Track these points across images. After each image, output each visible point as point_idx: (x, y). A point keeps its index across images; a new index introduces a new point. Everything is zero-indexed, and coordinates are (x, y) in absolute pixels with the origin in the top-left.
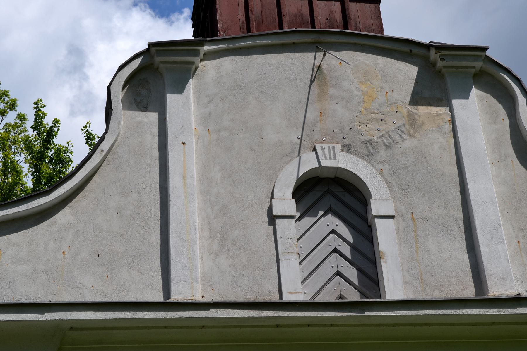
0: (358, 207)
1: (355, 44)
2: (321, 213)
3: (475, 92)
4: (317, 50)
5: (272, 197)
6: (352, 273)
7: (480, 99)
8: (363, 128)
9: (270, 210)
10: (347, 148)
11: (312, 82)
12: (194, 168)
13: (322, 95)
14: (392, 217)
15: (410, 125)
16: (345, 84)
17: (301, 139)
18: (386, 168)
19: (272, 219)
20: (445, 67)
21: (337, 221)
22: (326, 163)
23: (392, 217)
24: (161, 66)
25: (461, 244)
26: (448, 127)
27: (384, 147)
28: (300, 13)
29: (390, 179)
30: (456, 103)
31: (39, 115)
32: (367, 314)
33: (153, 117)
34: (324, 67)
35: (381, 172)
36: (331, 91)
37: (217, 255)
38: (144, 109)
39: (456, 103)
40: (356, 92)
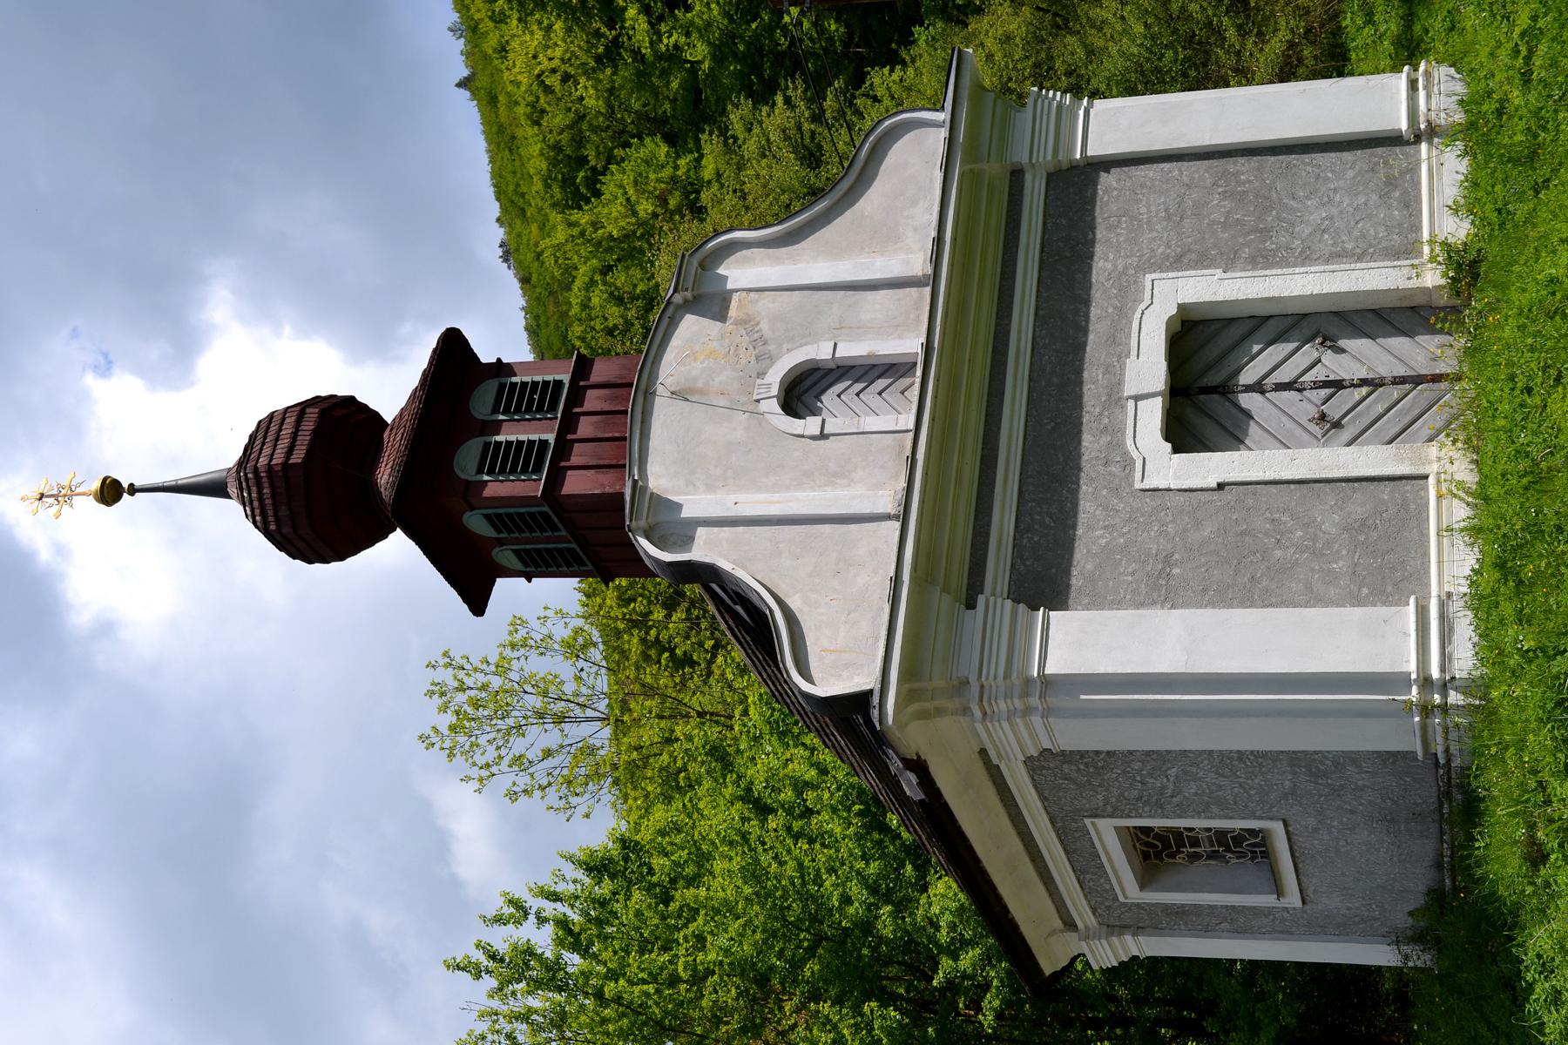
0: (817, 375)
1: (653, 362)
2: (819, 404)
3: (721, 271)
4: (654, 393)
5: (803, 436)
6: (881, 383)
7: (728, 268)
8: (743, 362)
9: (814, 438)
10: (761, 375)
11: (688, 400)
12: (761, 496)
13: (702, 392)
14: (835, 344)
15: (746, 324)
16: (694, 373)
17: (745, 412)
18: (785, 346)
19: (823, 436)
20: (693, 290)
21: (830, 391)
22: (775, 391)
23: (835, 344)
24: (650, 520)
25: (869, 295)
26: (752, 295)
27: (765, 346)
28: (595, 424)
29: (798, 344)
30: (730, 286)
31: (499, 920)
32: (936, 345)
33: (701, 532)
34: (672, 390)
35: (789, 350)
36: (700, 384)
37: (852, 481)
38: (692, 539)
39: (730, 286)
40: (705, 365)
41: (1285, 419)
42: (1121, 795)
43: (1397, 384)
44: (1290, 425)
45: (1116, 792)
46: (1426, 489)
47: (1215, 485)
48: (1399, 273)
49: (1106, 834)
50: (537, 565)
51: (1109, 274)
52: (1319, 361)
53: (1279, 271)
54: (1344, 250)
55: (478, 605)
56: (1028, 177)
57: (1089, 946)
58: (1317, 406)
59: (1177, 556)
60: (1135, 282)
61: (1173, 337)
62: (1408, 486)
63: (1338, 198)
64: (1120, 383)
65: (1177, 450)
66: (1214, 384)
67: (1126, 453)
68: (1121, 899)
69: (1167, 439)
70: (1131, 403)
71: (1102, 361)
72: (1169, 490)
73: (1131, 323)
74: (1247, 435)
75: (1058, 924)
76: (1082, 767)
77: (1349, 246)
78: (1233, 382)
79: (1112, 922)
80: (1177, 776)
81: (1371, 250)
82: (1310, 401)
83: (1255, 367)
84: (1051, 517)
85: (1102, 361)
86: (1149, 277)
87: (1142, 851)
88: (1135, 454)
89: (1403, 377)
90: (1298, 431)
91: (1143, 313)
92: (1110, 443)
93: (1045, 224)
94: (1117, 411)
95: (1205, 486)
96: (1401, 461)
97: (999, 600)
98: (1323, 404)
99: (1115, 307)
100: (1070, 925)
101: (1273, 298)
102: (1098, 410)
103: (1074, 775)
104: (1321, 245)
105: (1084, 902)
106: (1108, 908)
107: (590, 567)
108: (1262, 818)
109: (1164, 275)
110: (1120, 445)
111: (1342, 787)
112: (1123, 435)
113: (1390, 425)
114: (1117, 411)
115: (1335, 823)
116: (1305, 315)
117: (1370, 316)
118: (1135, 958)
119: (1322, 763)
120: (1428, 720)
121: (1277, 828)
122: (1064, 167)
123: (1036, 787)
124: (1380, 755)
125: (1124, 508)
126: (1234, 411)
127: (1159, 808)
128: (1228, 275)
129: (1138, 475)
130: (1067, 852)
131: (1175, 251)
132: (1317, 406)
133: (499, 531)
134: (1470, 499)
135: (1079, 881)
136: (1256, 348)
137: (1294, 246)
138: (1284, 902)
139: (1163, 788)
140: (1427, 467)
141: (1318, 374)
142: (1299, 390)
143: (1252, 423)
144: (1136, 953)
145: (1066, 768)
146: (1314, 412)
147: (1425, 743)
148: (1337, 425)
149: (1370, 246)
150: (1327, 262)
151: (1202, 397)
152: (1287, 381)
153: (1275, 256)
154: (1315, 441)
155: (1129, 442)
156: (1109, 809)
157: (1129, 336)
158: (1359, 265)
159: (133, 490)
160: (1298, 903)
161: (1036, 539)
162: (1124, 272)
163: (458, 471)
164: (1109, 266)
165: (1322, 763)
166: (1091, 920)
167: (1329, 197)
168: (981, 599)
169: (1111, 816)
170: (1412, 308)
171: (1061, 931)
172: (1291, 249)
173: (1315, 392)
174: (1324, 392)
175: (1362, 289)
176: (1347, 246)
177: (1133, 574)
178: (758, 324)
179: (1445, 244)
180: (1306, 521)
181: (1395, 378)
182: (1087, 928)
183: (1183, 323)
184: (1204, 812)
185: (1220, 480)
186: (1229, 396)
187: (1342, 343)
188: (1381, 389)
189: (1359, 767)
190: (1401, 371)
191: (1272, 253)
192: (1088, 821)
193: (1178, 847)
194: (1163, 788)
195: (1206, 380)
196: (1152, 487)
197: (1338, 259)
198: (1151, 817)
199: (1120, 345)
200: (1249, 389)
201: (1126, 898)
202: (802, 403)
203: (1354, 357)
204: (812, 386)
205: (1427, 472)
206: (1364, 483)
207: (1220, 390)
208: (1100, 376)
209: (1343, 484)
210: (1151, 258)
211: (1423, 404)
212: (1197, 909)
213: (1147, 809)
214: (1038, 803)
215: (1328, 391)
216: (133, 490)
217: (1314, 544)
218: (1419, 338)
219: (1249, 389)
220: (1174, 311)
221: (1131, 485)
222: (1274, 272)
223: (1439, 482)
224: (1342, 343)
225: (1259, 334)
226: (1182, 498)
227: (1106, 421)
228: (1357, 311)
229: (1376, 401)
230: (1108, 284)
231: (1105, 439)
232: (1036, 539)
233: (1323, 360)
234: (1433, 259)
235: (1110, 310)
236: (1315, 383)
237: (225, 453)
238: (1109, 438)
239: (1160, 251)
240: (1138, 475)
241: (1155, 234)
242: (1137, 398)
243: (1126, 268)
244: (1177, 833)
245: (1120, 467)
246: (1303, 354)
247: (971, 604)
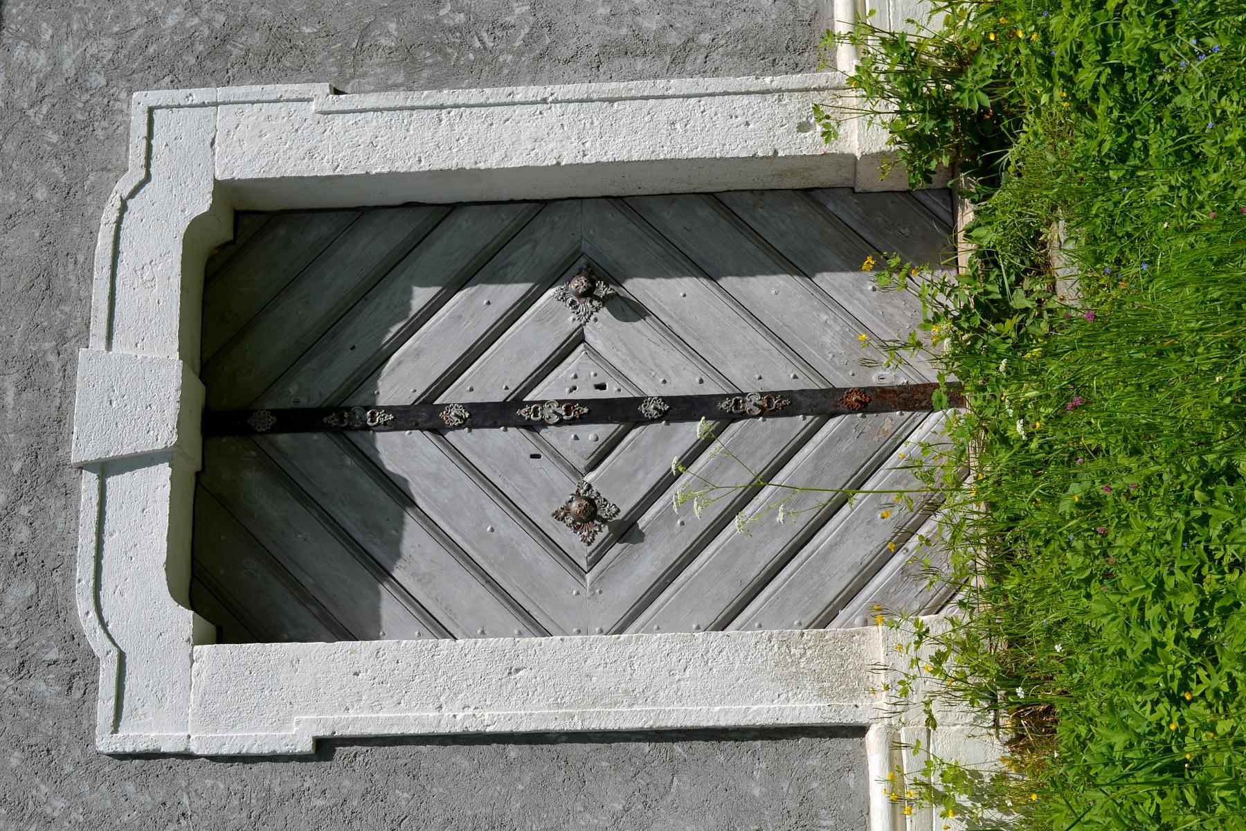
41: (494, 510)
43: (776, 413)
44: (509, 528)
46: (858, 765)
47: (306, 746)
48: (780, 112)
51: (41, 85)
52: (577, 340)
53: (474, 95)
54: (637, 34)
58: (574, 471)
60: (107, 111)
61: (211, 260)
62: (814, 756)
64: (61, 419)
66: (315, 402)
67: (74, 637)
70: (89, 482)
71: (16, 349)
72: (188, 756)
73: (93, 234)
74: (398, 555)
77: (650, 24)
78: (361, 399)
81: (705, 38)
82: (557, 456)
83: (417, 353)
85: (16, 349)
86: (142, 99)
88: (97, 642)
89: (784, 394)
91: (124, 208)
92: (31, 604)
94: (54, 503)
95: (282, 749)
96: (793, 681)
98: (592, 467)
99: (54, 187)
101: (460, 172)
104: (579, 19)
109: (179, 95)
110: (61, 610)
112: (68, 579)
114: (54, 503)
117: (705, 212)
125: (66, 813)
126: (366, 483)
128: (343, 102)
129: (104, 708)
131: (209, 22)
132: (574, 471)
136: (421, 296)
137: (510, 19)
140: (864, 703)
142: (532, 427)
143: (411, 521)
146: (564, 487)
148: (627, 531)
149: (703, 25)
150: (596, 69)
151: (284, 440)
152: (498, 396)
153: (463, 46)
155: (84, 604)
157: (86, 277)
158: (677, 84)
162: (77, 82)
164: (40, 60)
170: (807, 191)
172: (504, 27)
173: (569, 431)
175: (685, 154)
176: (646, 24)
179: (894, 43)
181: (769, 396)
183: (239, 216)
185: (321, 733)
186: (353, 436)
187: (638, 288)
188: (735, 427)
191: (455, 39)
195: (293, 389)
196: (141, 747)
197: (624, 61)
199: (61, 301)
200: (403, 418)
203: (666, 329)
205: (862, 720)
206: (700, 745)
209: (646, 747)
210: (148, 39)
211: (841, 475)
215: (604, 431)
218: (826, 280)
219: (403, 418)
220: (203, 204)
221: (86, 739)
222: (462, 96)
223: (894, 746)
224: (638, 288)
225: (431, 254)
226: (218, 783)
227: (23, 533)
228: (671, 197)
229: (729, 456)
230: (37, 116)
233: (589, 338)
234: (864, 81)
235: (41, 194)
236: (569, 405)
238: (30, 589)
239: (171, 21)
240: (104, 708)
242: (105, 468)
243: (83, 69)
245: (58, 680)
246: (539, 319)
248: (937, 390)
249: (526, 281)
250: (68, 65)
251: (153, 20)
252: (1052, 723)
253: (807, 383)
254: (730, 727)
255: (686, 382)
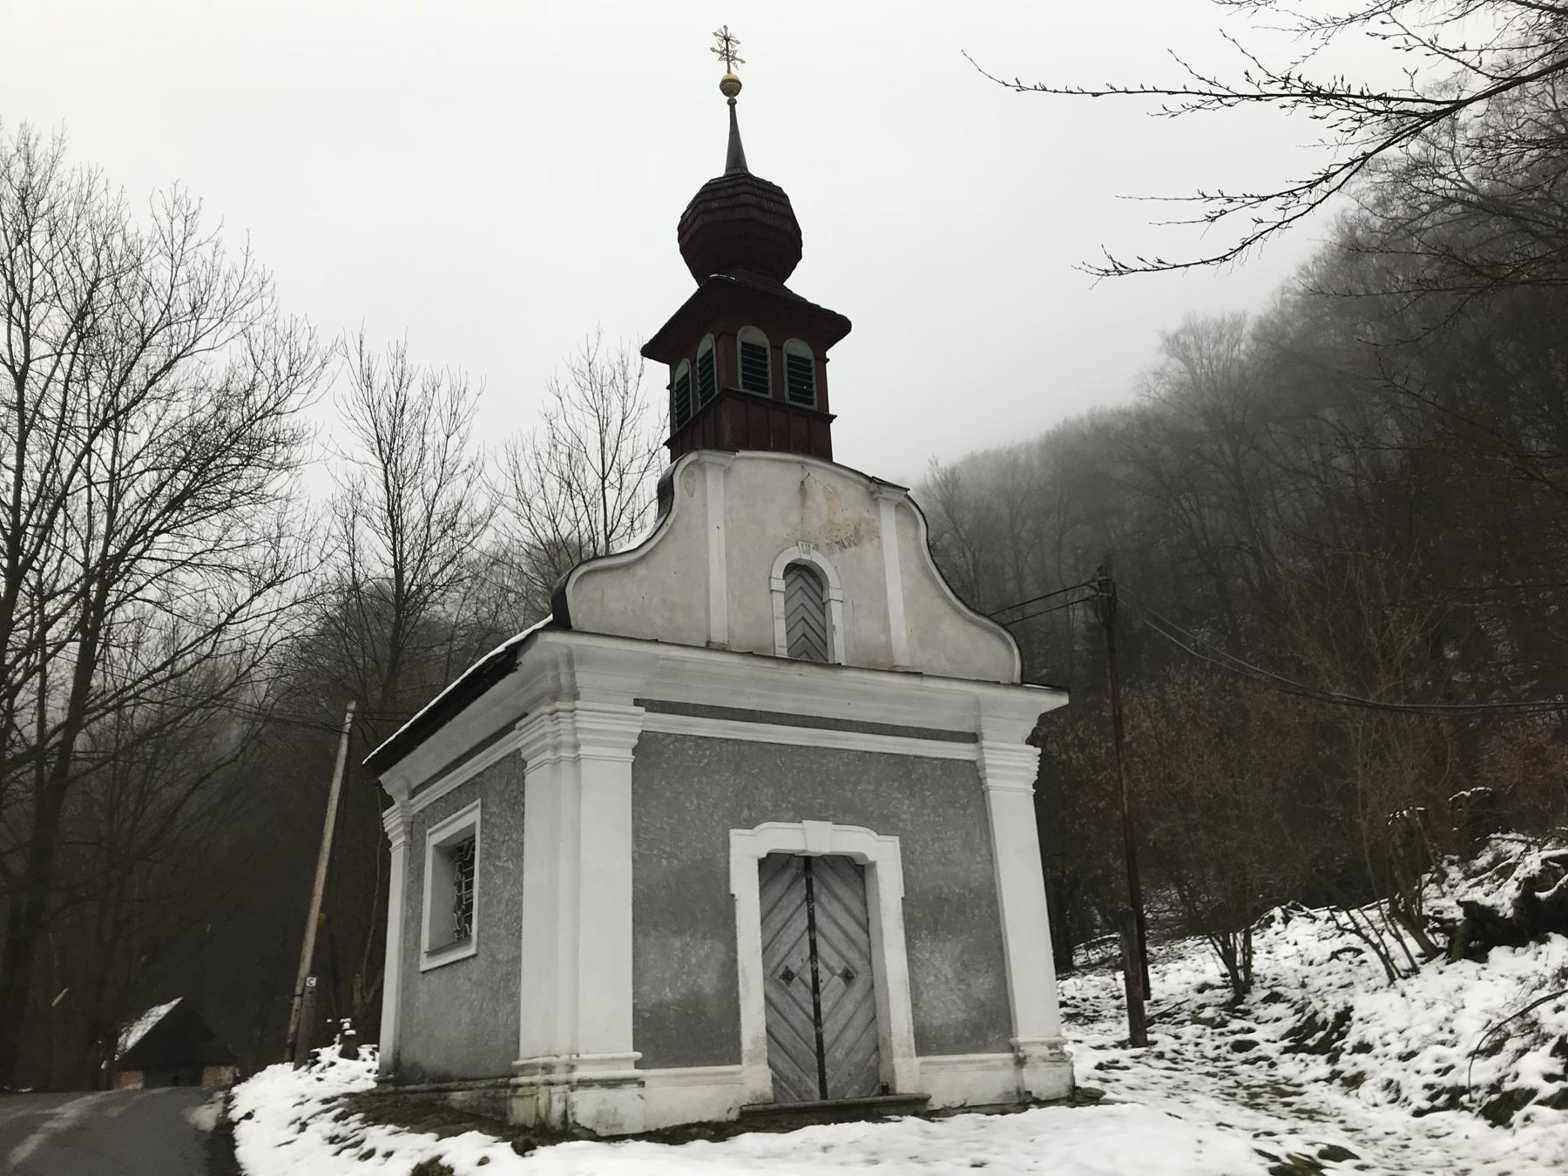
0: (818, 589)
22: (806, 557)
36: (809, 503)
42: (496, 826)
45: (498, 821)
47: (732, 892)
49: (470, 817)
50: (677, 392)
55: (650, 351)
56: (972, 746)
57: (398, 808)
59: (676, 862)
61: (851, 858)
63: (962, 987)
65: (762, 863)
68: (429, 831)
69: (769, 854)
75: (414, 784)
76: (515, 793)
79: (414, 825)
80: (508, 868)
84: (707, 764)
87: (462, 847)
90: (778, 959)
93: (936, 759)
97: (640, 724)
100: (414, 793)
102: (793, 799)
103: (510, 787)
105: (427, 803)
106: (424, 822)
107: (677, 430)
108: (478, 937)
111: (498, 1000)
113: (783, 1033)
114: (792, 814)
115: (474, 995)
116: (870, 962)
117: (871, 1015)
118: (390, 844)
119: (514, 984)
120: (540, 1070)
121: (471, 951)
122: (980, 774)
123: (503, 759)
124: (517, 1032)
127: (487, 856)
130: (460, 787)
133: (700, 361)
134: (1256, 582)
135: (441, 798)
138: (423, 957)
139: (499, 858)
141: (824, 974)
142: (811, 958)
144: (393, 845)
145: (514, 781)
147: (523, 1067)
151: (804, 881)
154: (769, 972)
156: (487, 817)
159: (732, 104)
160: (423, 967)
161: (691, 752)
163: (743, 329)
164: (905, 808)
165: (514, 984)
166: (416, 810)
167: (963, 980)
168: (642, 710)
169: (482, 819)
171: (409, 787)
174: (809, 978)
177: (662, 828)
178: (856, 545)
180: (704, 966)
182: (412, 806)
184: (483, 892)
189: (511, 1014)
190: (827, 1040)
192: (479, 801)
193: (464, 873)
194: (499, 858)
198: (481, 848)
201: (430, 834)
202: (796, 578)
204: (809, 585)
207: (810, 896)
208: (819, 801)
212: (421, 890)
213: (486, 846)
214: (491, 763)
216: (732, 104)
217: (685, 973)
220: (871, 858)
231: (769, 805)
232: (691, 752)
235: (871, 809)
237: (757, 167)
241: (930, 843)
244: (471, 873)
247: (637, 702)
248: (1461, 900)
249: (1055, 687)
250: (904, 816)
251: (917, 842)
252: (1391, 794)
253: (826, 1046)
254: (756, 344)
255: (824, 1008)
